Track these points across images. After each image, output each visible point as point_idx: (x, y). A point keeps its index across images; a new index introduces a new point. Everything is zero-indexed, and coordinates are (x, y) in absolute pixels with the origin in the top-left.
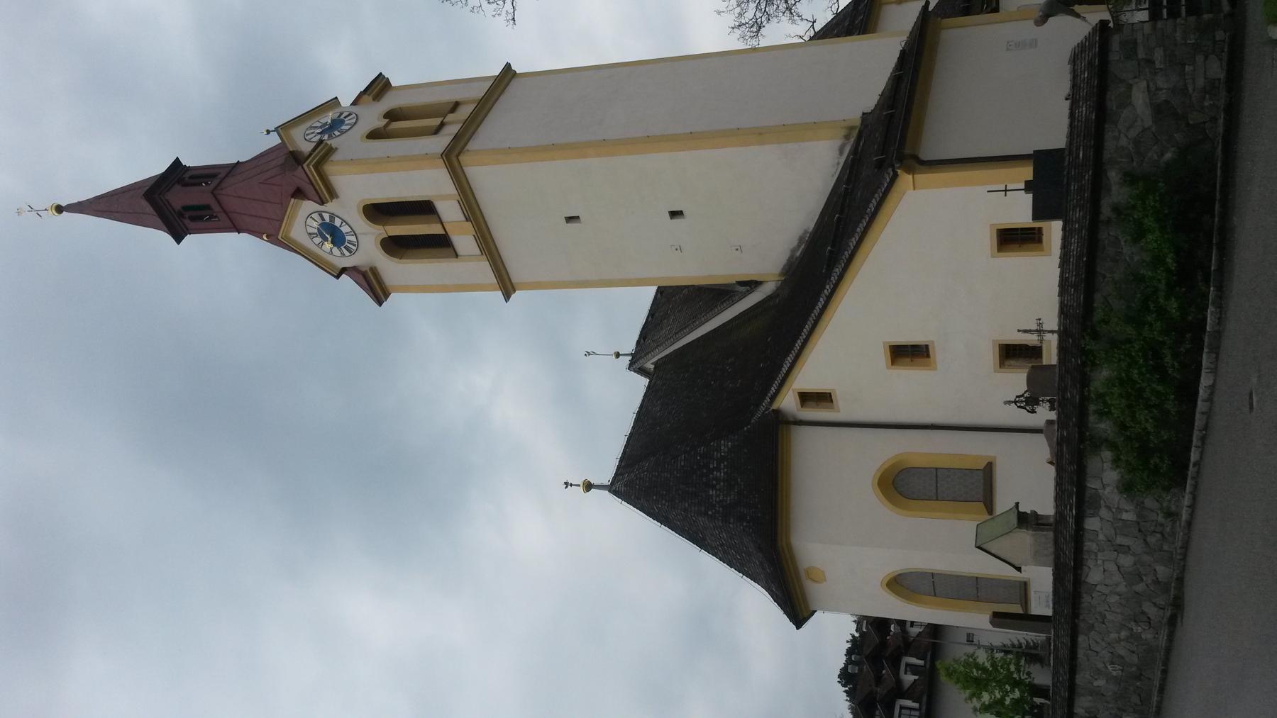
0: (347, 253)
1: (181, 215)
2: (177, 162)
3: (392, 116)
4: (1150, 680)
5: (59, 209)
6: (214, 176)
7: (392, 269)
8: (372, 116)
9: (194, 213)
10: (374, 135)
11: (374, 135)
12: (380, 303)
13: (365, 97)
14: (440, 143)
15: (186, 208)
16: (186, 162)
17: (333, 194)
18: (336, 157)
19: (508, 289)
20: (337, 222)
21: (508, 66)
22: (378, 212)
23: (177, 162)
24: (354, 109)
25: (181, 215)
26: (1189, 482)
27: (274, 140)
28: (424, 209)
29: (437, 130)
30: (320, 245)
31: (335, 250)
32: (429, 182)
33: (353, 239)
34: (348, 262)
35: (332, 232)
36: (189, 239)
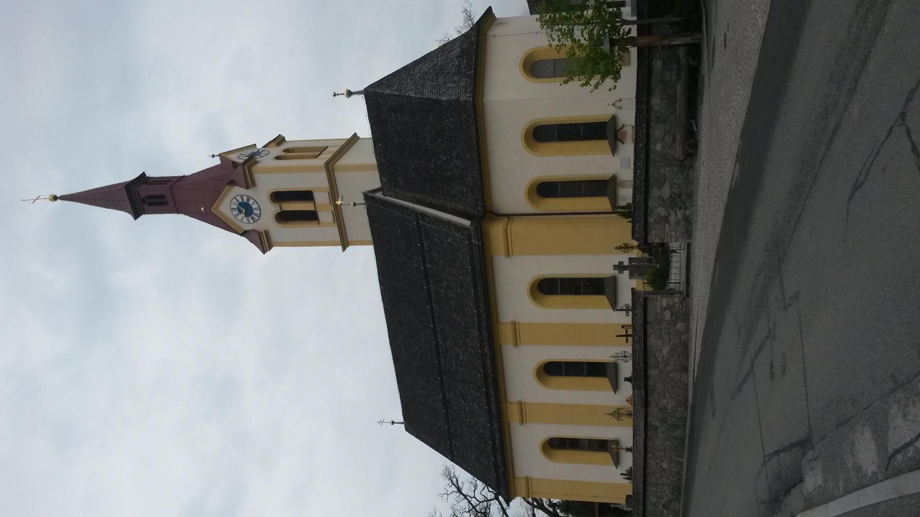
0: (251, 221)
1: (143, 201)
2: (143, 174)
3: (286, 151)
4: (682, 490)
5: (55, 198)
7: (277, 230)
8: (277, 151)
9: (151, 201)
10: (278, 158)
11: (278, 158)
12: (264, 253)
13: (272, 144)
15: (149, 197)
17: (254, 184)
18: (259, 165)
19: (345, 244)
20: (251, 202)
21: (355, 134)
22: (278, 197)
23: (143, 174)
25: (143, 201)
26: (689, 410)
27: (217, 161)
28: (307, 196)
30: (236, 216)
31: (245, 220)
32: (316, 182)
33: (258, 212)
35: (246, 208)
36: (144, 218)
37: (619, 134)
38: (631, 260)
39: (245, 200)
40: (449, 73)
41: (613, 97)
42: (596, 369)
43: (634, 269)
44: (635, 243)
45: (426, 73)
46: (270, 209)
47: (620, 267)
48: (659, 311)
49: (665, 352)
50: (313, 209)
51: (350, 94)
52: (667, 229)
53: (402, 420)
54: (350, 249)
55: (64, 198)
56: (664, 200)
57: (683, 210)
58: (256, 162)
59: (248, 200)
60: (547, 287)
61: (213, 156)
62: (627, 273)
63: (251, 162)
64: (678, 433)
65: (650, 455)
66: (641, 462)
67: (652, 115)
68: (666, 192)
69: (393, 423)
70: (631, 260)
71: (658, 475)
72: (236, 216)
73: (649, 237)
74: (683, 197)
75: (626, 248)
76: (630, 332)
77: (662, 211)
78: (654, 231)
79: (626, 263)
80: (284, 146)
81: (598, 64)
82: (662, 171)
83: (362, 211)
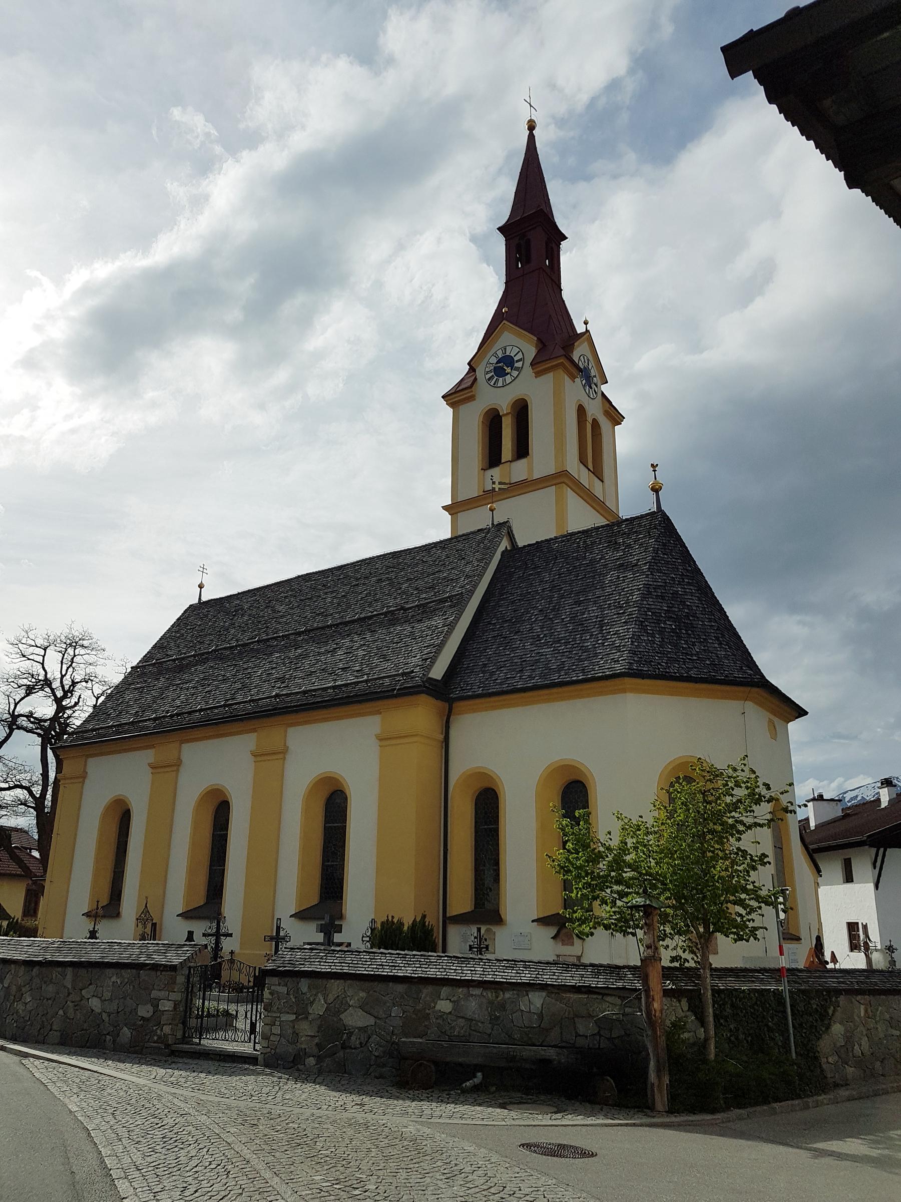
0: (488, 376)
5: (531, 126)
6: (597, 472)
7: (475, 412)
8: (594, 410)
10: (581, 410)
11: (581, 410)
14: (573, 466)
16: (564, 244)
17: (538, 374)
22: (521, 411)
24: (600, 394)
27: (580, 329)
28: (522, 450)
29: (583, 460)
32: (542, 459)
33: (500, 384)
34: (480, 373)
35: (505, 366)
39: (516, 359)
40: (680, 638)
45: (683, 603)
46: (501, 398)
48: (155, 994)
49: (95, 1004)
51: (656, 490)
52: (284, 1017)
53: (204, 599)
54: (447, 517)
55: (531, 139)
56: (339, 1012)
57: (315, 1051)
58: (573, 378)
59: (517, 369)
60: (334, 806)
61: (586, 323)
63: (574, 371)
67: (508, 995)
69: (201, 586)
73: (275, 980)
74: (341, 1054)
77: (318, 1008)
78: (284, 990)
80: (604, 422)
82: (395, 1011)
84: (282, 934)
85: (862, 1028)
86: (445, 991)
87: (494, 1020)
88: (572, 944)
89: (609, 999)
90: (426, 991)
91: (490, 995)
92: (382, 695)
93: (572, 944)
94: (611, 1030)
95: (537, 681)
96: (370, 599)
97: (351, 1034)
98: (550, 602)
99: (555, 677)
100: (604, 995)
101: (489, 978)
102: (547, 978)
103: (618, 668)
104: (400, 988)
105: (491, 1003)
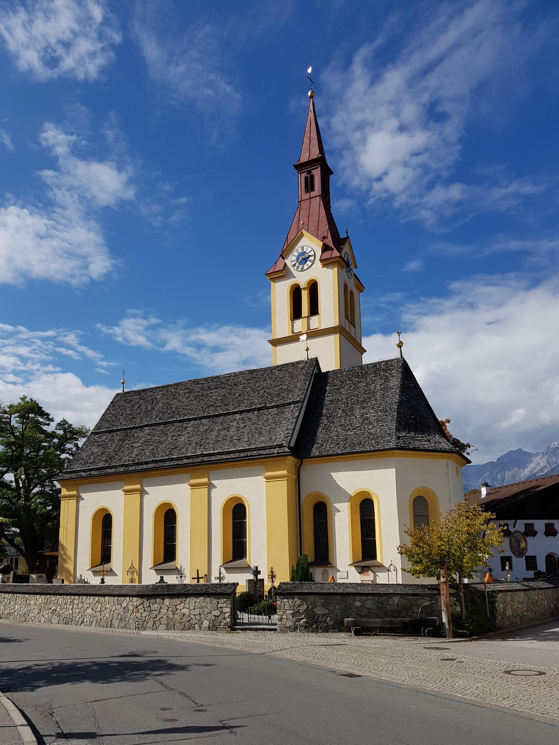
1: (309, 172)
2: (332, 173)
8: (351, 285)
21: (366, 351)
22: (313, 287)
23: (332, 173)
28: (314, 310)
30: (297, 251)
37: (367, 569)
38: (262, 581)
41: (393, 567)
42: (168, 551)
43: (256, 584)
44: (276, 584)
46: (302, 279)
47: (257, 572)
50: (303, 316)
53: (514, 521)
62: (252, 577)
64: (116, 623)
65: (97, 598)
66: (91, 591)
68: (320, 611)
70: (262, 581)
71: (80, 605)
72: (297, 251)
75: (272, 576)
76: (202, 582)
79: (259, 577)
80: (355, 292)
81: (419, 555)
83: (301, 356)
84: (222, 576)
85: (509, 605)
86: (358, 598)
87: (379, 608)
88: (369, 575)
89: (425, 598)
90: (350, 599)
91: (376, 598)
92: (266, 456)
93: (369, 575)
94: (426, 610)
95: (348, 450)
96: (241, 398)
97: (318, 617)
98: (348, 406)
99: (358, 449)
100: (423, 596)
101: (376, 592)
102: (398, 591)
103: (392, 445)
104: (338, 597)
105: (377, 602)
